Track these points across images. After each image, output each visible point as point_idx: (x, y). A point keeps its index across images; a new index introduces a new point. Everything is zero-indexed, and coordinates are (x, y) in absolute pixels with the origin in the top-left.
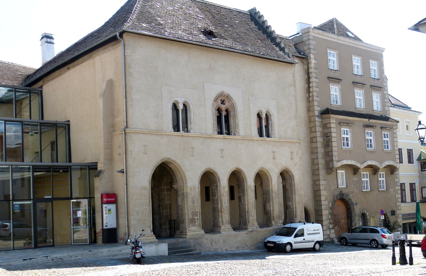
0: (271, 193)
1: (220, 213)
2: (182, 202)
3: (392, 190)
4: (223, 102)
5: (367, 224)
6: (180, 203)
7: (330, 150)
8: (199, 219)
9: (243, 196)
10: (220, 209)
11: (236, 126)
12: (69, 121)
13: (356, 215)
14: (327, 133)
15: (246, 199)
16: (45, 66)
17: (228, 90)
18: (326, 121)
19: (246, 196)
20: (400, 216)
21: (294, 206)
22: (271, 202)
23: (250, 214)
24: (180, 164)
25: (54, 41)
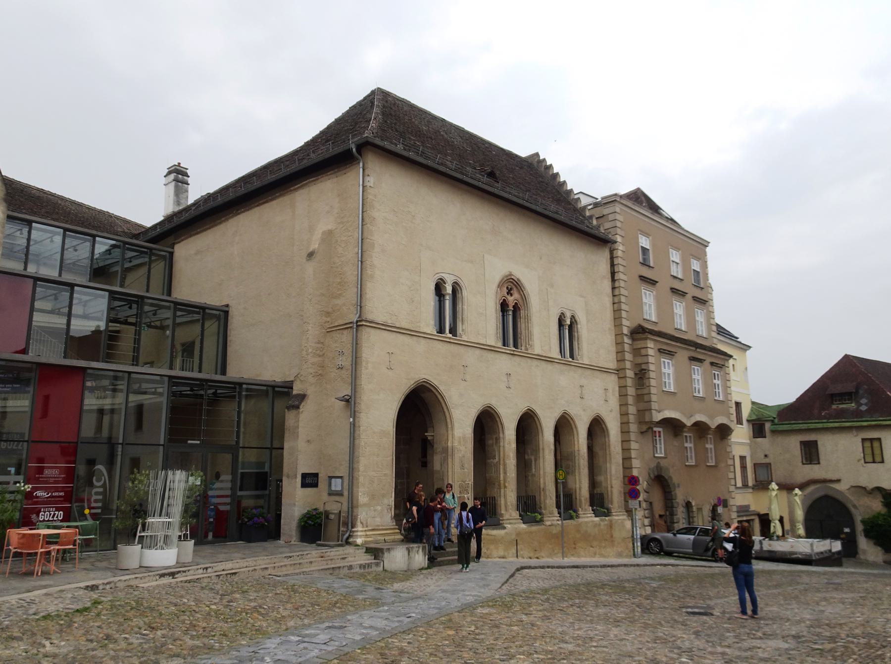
0: (577, 458)
1: (502, 491)
2: (441, 465)
3: (723, 465)
4: (509, 292)
5: (693, 520)
6: (437, 466)
7: (645, 391)
8: (470, 499)
9: (536, 460)
10: (502, 482)
11: (530, 336)
12: (227, 306)
13: (678, 503)
14: (640, 364)
15: (541, 465)
16: (169, 219)
17: (520, 273)
18: (640, 344)
19: (541, 460)
20: (735, 509)
21: (609, 482)
22: (577, 474)
23: (547, 493)
24: (444, 393)
25: (190, 180)
